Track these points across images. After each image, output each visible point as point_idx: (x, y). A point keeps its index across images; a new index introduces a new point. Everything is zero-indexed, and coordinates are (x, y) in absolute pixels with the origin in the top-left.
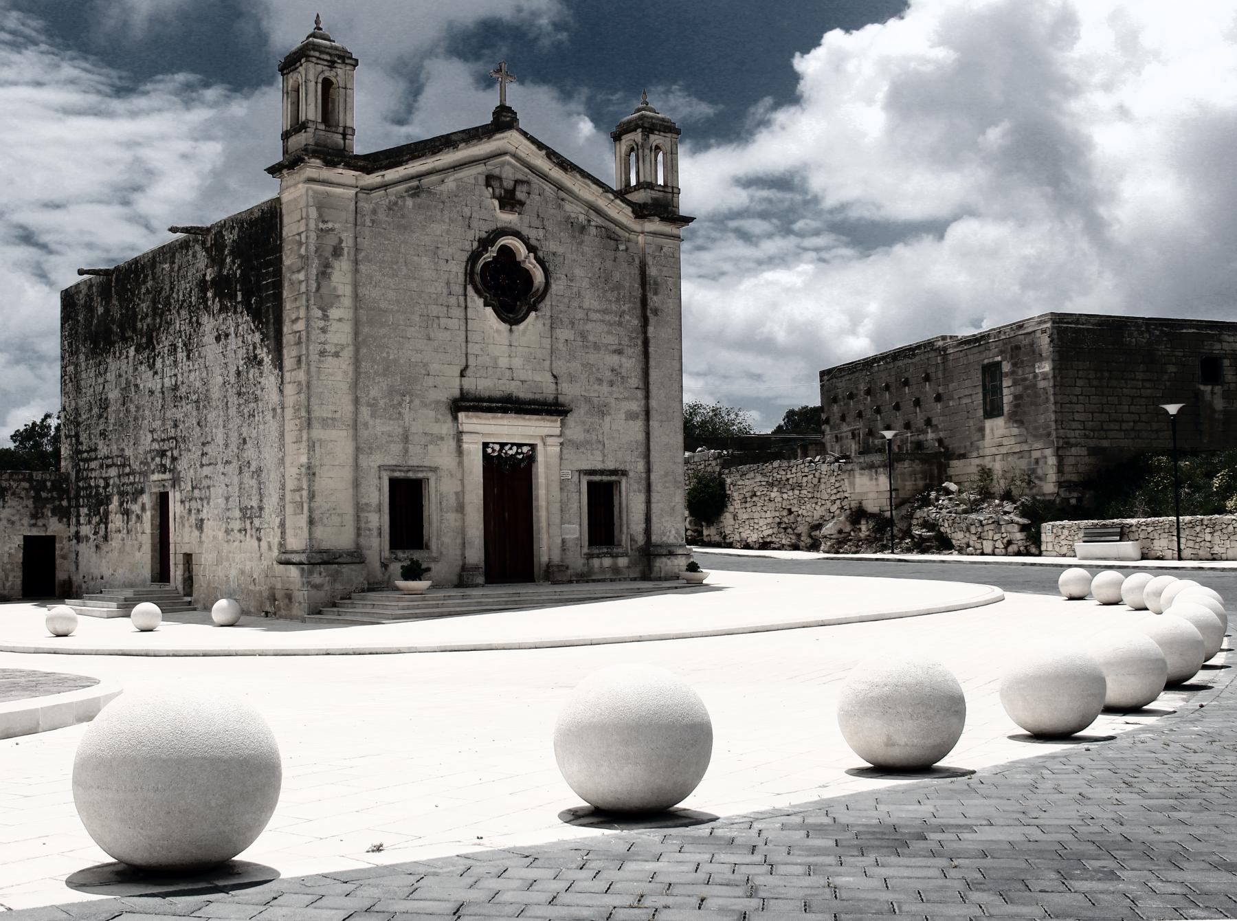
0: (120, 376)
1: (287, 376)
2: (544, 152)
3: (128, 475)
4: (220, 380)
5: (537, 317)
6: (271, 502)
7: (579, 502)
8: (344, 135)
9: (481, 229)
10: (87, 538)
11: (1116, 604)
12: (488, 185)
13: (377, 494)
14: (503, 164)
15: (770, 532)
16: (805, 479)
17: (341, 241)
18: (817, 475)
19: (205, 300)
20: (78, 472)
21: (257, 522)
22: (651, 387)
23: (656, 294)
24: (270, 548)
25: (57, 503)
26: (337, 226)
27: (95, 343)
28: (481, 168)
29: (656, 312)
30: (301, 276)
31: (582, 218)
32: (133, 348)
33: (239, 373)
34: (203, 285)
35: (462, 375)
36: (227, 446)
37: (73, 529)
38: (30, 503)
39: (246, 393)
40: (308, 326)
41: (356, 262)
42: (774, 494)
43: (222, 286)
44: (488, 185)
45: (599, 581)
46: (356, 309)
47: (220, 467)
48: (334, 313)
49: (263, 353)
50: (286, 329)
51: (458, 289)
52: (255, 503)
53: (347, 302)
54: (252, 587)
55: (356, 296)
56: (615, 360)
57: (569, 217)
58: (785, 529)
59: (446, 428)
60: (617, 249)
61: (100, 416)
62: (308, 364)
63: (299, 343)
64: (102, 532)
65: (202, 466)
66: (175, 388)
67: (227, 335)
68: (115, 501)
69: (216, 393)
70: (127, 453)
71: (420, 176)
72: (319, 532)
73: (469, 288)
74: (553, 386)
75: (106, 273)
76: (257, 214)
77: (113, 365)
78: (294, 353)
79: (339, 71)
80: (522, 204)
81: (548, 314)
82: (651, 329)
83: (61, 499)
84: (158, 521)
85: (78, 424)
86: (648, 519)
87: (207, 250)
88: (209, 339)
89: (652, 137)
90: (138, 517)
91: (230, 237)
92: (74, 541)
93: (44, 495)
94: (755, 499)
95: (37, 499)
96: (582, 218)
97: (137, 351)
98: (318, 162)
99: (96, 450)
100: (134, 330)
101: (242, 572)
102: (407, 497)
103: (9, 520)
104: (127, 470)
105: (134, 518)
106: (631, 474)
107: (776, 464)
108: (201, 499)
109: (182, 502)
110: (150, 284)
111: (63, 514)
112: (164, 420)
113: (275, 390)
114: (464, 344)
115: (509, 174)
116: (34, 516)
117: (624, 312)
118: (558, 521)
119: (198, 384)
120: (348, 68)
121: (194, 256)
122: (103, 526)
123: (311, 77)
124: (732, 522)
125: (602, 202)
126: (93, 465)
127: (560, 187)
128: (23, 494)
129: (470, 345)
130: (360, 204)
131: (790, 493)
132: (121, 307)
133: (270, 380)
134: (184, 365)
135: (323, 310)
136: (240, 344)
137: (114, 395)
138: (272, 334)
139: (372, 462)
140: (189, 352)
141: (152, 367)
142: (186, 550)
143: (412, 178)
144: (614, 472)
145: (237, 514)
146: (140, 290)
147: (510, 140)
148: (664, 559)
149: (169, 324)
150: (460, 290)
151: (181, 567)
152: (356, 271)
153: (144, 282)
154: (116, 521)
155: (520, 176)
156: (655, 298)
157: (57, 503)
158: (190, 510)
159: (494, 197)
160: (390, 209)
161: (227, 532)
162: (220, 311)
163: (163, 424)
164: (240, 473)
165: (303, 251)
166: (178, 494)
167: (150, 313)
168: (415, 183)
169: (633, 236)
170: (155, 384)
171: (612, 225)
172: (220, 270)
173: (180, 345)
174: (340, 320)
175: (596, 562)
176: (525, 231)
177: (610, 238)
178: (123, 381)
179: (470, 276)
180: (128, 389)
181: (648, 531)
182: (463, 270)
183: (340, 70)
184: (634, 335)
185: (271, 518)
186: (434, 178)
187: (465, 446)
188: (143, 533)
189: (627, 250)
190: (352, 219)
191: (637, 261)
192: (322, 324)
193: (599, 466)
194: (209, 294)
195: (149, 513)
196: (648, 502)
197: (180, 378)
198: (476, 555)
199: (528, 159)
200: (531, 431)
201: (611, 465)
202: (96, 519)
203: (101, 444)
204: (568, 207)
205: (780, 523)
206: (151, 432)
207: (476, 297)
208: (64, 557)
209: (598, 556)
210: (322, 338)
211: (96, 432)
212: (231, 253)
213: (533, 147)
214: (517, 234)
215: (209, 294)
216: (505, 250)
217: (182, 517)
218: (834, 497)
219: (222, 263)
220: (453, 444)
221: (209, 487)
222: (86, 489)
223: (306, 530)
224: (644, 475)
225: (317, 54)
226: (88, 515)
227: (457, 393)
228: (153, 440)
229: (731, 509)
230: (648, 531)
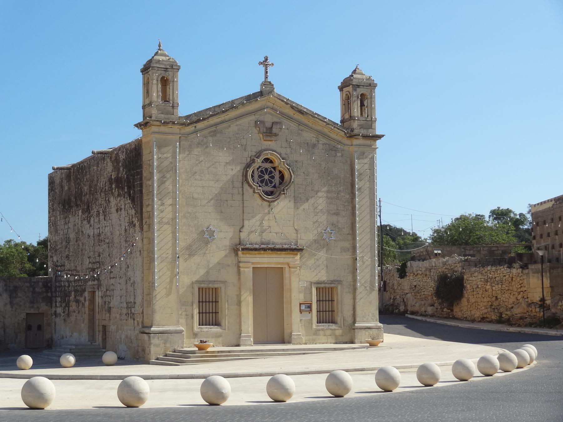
0: (75, 225)
1: (145, 233)
4: (118, 232)
9: (252, 151)
10: (60, 314)
15: (486, 311)
16: (504, 278)
18: (511, 276)
19: (112, 190)
20: (56, 277)
21: (133, 310)
24: (138, 324)
25: (45, 294)
28: (253, 118)
32: (80, 211)
33: (126, 230)
34: (110, 181)
36: (121, 268)
37: (54, 309)
43: (118, 181)
49: (135, 221)
51: (238, 184)
52: (132, 300)
58: (494, 309)
64: (67, 312)
65: (110, 278)
66: (99, 235)
67: (121, 209)
68: (73, 293)
69: (116, 240)
70: (79, 268)
71: (216, 125)
75: (68, 169)
77: (72, 219)
80: (276, 135)
83: (47, 292)
88: (113, 210)
91: (122, 157)
92: (54, 316)
94: (478, 290)
96: (314, 140)
97: (82, 212)
98: (158, 123)
99: (64, 266)
100: (81, 201)
101: (127, 336)
105: (81, 304)
106: (344, 283)
108: (110, 296)
109: (102, 297)
110: (88, 176)
112: (94, 252)
115: (269, 119)
116: (32, 302)
117: (340, 191)
119: (109, 234)
120: (175, 70)
122: (67, 308)
124: (466, 304)
127: (300, 123)
129: (245, 214)
131: (497, 286)
132: (76, 188)
136: (126, 215)
137: (72, 236)
138: (139, 211)
140: (105, 216)
141: (89, 222)
142: (104, 323)
145: (125, 305)
146: (84, 179)
149: (96, 199)
150: (240, 185)
151: (101, 333)
153: (86, 175)
154: (73, 306)
155: (276, 120)
157: (45, 294)
158: (105, 302)
162: (119, 195)
163: (94, 254)
166: (100, 293)
167: (88, 193)
168: (213, 129)
169: (346, 148)
170: (90, 232)
172: (118, 174)
173: (101, 212)
176: (279, 150)
177: (331, 150)
180: (79, 232)
182: (241, 174)
184: (346, 204)
186: (224, 125)
187: (242, 269)
188: (85, 313)
189: (342, 156)
191: (349, 162)
194: (114, 186)
197: (101, 230)
200: (281, 260)
202: (64, 305)
203: (66, 262)
205: (491, 305)
206: (89, 258)
207: (249, 188)
211: (64, 255)
212: (123, 165)
215: (114, 186)
217: (102, 305)
218: (519, 290)
219: (119, 170)
220: (235, 269)
221: (113, 290)
224: (352, 283)
226: (60, 302)
228: (90, 262)
229: (466, 295)
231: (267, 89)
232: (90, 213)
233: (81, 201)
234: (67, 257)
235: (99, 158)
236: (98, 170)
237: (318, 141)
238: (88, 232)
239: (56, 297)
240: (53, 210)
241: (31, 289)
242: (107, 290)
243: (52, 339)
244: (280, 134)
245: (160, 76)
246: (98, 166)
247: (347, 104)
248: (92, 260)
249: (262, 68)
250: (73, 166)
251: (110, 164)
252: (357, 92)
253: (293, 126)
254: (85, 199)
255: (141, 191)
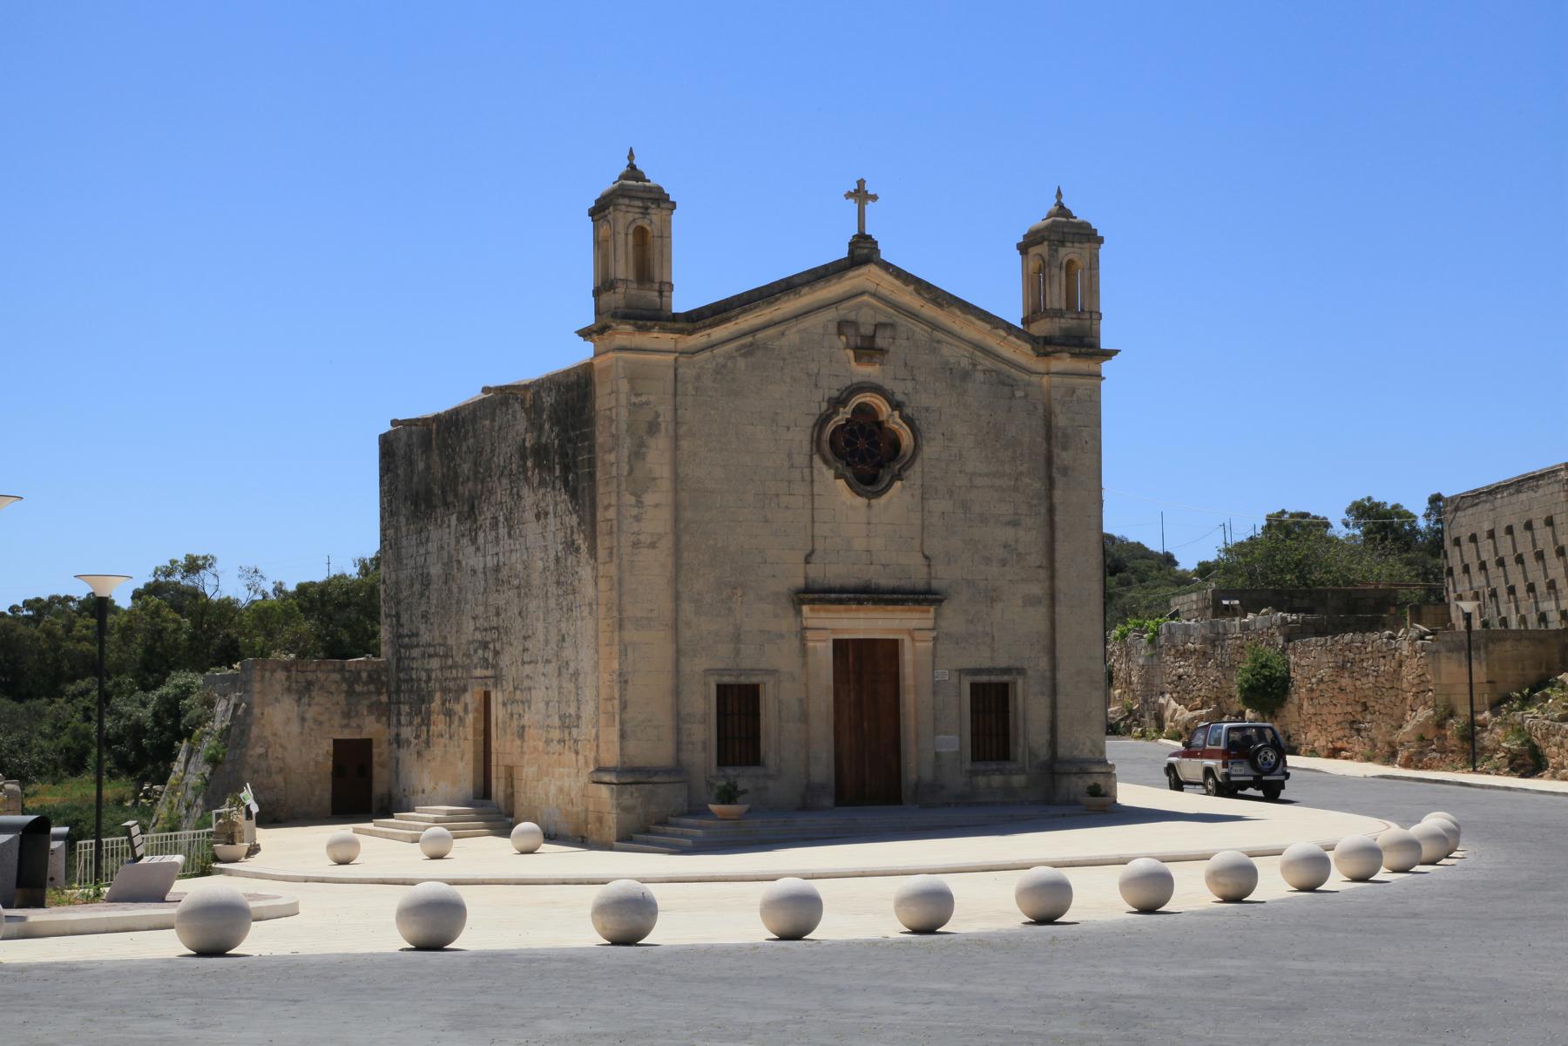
1: (601, 567)
2: (911, 288)
3: (451, 667)
4: (540, 564)
5: (903, 487)
6: (588, 710)
7: (959, 707)
8: (661, 293)
9: (832, 388)
11: (532, 852)
12: (840, 332)
13: (702, 703)
14: (859, 307)
15: (1340, 734)
17: (657, 415)
19: (525, 471)
20: (399, 660)
21: (574, 731)
22: (1057, 565)
23: (1065, 448)
25: (374, 698)
26: (652, 398)
27: (416, 504)
28: (831, 315)
29: (1065, 471)
30: (612, 457)
31: (965, 362)
33: (557, 560)
35: (807, 560)
36: (547, 642)
37: (394, 730)
38: (342, 698)
39: (565, 583)
40: (619, 513)
41: (676, 438)
42: (1345, 681)
43: (540, 453)
44: (840, 332)
45: (986, 804)
46: (676, 491)
47: (540, 666)
48: (649, 499)
50: (599, 515)
51: (801, 460)
52: (572, 711)
53: (666, 485)
54: (569, 808)
55: (676, 478)
56: (1009, 534)
57: (947, 363)
59: (787, 623)
60: (1013, 396)
61: (422, 595)
62: (621, 559)
63: (611, 533)
64: (424, 736)
65: (524, 663)
66: (497, 569)
67: (546, 514)
68: (438, 696)
69: (536, 579)
70: (451, 641)
71: (753, 331)
72: (631, 745)
73: (817, 459)
74: (925, 570)
76: (573, 378)
77: (435, 533)
78: (607, 544)
79: (654, 218)
80: (882, 351)
81: (919, 482)
82: (1058, 494)
83: (380, 693)
84: (481, 726)
85: (398, 603)
86: (1053, 729)
87: (527, 411)
88: (529, 515)
89: (1062, 251)
90: (461, 719)
91: (548, 400)
93: (358, 688)
94: (1322, 686)
95: (350, 693)
96: (965, 362)
98: (628, 328)
99: (417, 635)
100: (456, 495)
101: (561, 790)
102: (739, 708)
103: (315, 720)
104: (450, 662)
106: (1030, 673)
107: (1348, 637)
109: (504, 704)
110: (471, 441)
111: (384, 712)
113: (591, 582)
114: (809, 525)
115: (867, 320)
116: (347, 715)
117: (1021, 473)
118: (934, 731)
119: (519, 567)
121: (514, 417)
123: (621, 228)
125: (993, 341)
126: (416, 652)
127: (935, 326)
128: (333, 688)
129: (817, 525)
130: (681, 371)
133: (586, 572)
134: (506, 543)
135: (637, 496)
137: (435, 570)
138: (588, 518)
139: (696, 666)
140: (511, 528)
141: (474, 541)
142: (508, 761)
143: (745, 334)
144: (1007, 671)
145: (556, 721)
147: (866, 277)
148: (1074, 779)
149: (491, 492)
150: (806, 461)
152: (676, 448)
153: (465, 439)
155: (882, 319)
156: (1064, 454)
157: (374, 698)
159: (848, 346)
160: (717, 373)
161: (548, 742)
163: (486, 611)
164: (560, 674)
165: (613, 430)
168: (748, 339)
169: (1034, 378)
171: (1001, 366)
172: (539, 437)
173: (501, 519)
174: (657, 506)
175: (981, 781)
176: (889, 385)
177: (1003, 384)
178: (445, 555)
179: (816, 442)
180: (451, 564)
181: (1053, 743)
182: (808, 438)
183: (656, 215)
184: (1035, 502)
185: (586, 730)
186: (771, 332)
187: (810, 644)
189: (1026, 396)
190: (670, 390)
192: (635, 511)
193: (987, 664)
194: (529, 464)
195: (471, 716)
196: (1054, 707)
198: (823, 769)
199: (893, 297)
200: (896, 624)
201: (1003, 662)
202: (417, 720)
203: (422, 627)
204: (946, 351)
207: (824, 468)
208: (383, 765)
209: (984, 773)
210: (636, 527)
212: (550, 418)
213: (897, 283)
214: (877, 389)
215: (529, 464)
216: (862, 409)
217: (504, 722)
219: (541, 428)
220: (796, 643)
222: (406, 681)
223: (617, 745)
224: (1048, 674)
225: (626, 201)
227: (800, 582)
228: (476, 629)
229: (1295, 698)
230: (1053, 743)
231: (863, 251)
232: (475, 521)
233: (456, 495)
234: (425, 616)
235: (501, 398)
236: (492, 429)
237: (974, 365)
238: (471, 562)
239: (399, 703)
240: (392, 514)
241: (344, 687)
242: (515, 689)
243: (390, 795)
244: (892, 349)
245: (632, 214)
246: (493, 420)
247: (1035, 283)
248: (481, 623)
249: (852, 205)
250: (437, 418)
251: (521, 415)
252: (1061, 248)
253: (920, 331)
254: (464, 490)
255: (592, 476)
